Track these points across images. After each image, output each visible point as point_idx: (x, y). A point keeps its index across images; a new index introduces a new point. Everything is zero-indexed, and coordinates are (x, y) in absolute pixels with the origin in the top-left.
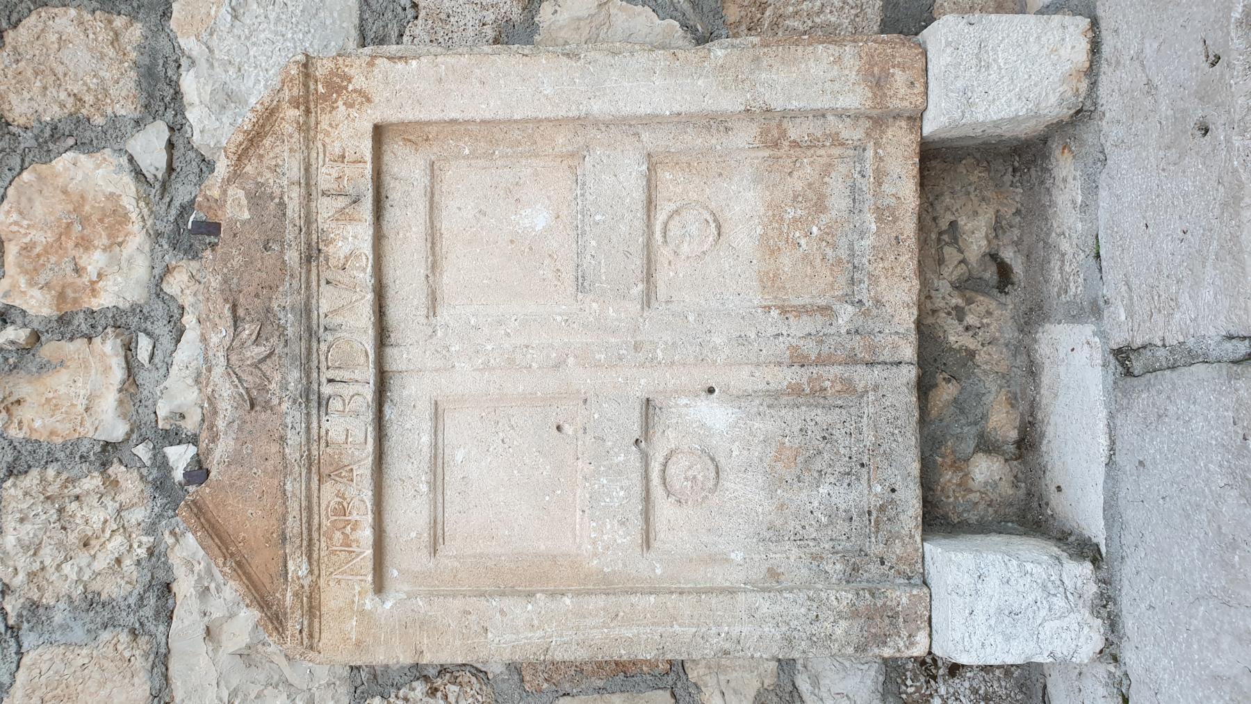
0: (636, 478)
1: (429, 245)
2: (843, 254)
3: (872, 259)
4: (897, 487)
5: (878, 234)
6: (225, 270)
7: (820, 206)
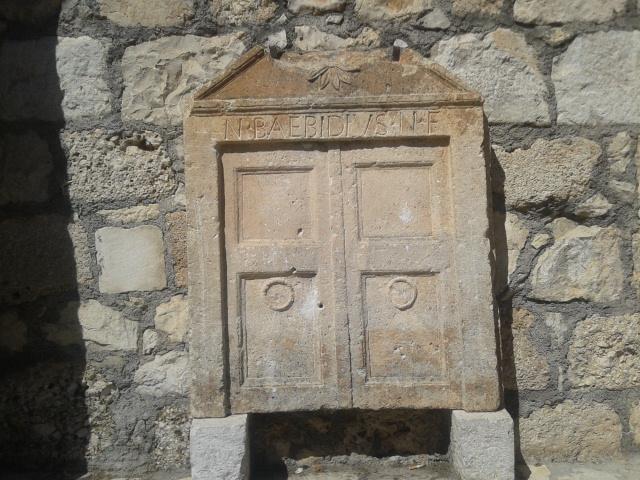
0: (276, 269)
2: (393, 371)
7: (416, 360)
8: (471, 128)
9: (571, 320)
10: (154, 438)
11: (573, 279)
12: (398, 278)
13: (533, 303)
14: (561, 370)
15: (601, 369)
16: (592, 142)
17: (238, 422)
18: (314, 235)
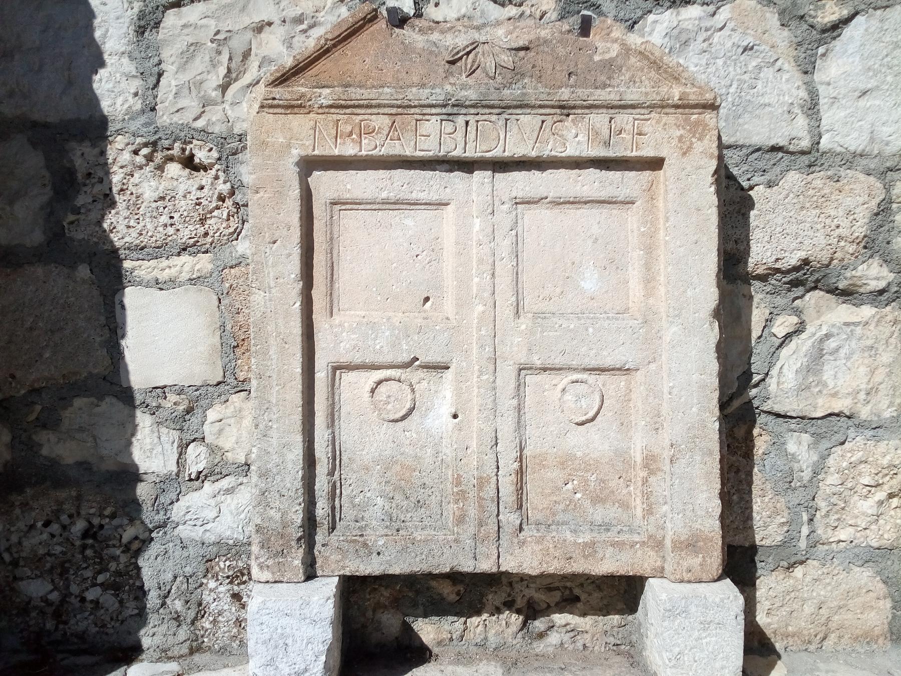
0: (388, 358)
1: (571, 200)
2: (560, 517)
3: (556, 539)
4: (381, 556)
5: (575, 543)
6: (554, 41)
7: (597, 500)
8: (698, 146)
9: (825, 444)
10: (200, 604)
11: (831, 384)
12: (576, 376)
13: (771, 418)
14: (805, 517)
15: (861, 519)
16: (871, 178)
17: (322, 597)
18: (449, 308)
